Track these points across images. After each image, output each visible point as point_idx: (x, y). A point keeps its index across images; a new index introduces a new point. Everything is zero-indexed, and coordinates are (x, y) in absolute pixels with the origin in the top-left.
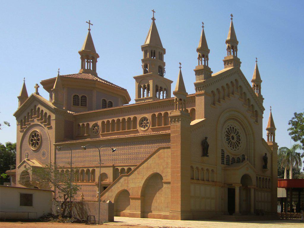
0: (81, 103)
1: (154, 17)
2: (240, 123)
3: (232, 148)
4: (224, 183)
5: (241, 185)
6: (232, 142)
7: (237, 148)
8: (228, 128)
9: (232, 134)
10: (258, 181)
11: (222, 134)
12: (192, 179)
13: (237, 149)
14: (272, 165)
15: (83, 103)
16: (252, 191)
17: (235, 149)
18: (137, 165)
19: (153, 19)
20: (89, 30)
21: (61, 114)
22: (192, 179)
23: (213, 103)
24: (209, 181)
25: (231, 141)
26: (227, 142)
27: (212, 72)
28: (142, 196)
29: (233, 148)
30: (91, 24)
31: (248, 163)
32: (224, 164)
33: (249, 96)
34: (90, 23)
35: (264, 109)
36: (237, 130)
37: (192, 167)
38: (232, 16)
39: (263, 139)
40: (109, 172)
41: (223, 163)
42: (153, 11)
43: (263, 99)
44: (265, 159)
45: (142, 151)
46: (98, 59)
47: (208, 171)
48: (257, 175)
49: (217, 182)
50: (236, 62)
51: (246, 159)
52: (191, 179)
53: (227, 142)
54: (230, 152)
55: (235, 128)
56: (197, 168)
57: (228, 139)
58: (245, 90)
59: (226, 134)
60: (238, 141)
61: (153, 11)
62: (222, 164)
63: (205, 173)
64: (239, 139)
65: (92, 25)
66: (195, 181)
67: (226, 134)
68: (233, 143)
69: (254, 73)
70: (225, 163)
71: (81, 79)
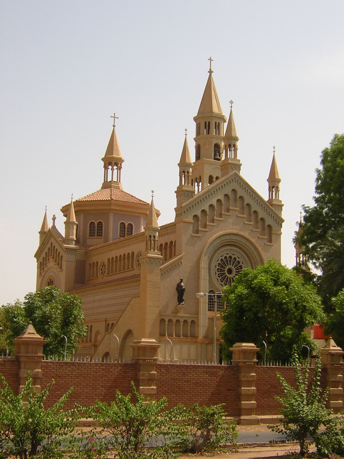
1: (210, 69)
8: (226, 257)
15: (99, 232)
19: (211, 72)
25: (228, 277)
30: (116, 118)
34: (114, 117)
42: (211, 60)
61: (211, 60)
65: (118, 118)
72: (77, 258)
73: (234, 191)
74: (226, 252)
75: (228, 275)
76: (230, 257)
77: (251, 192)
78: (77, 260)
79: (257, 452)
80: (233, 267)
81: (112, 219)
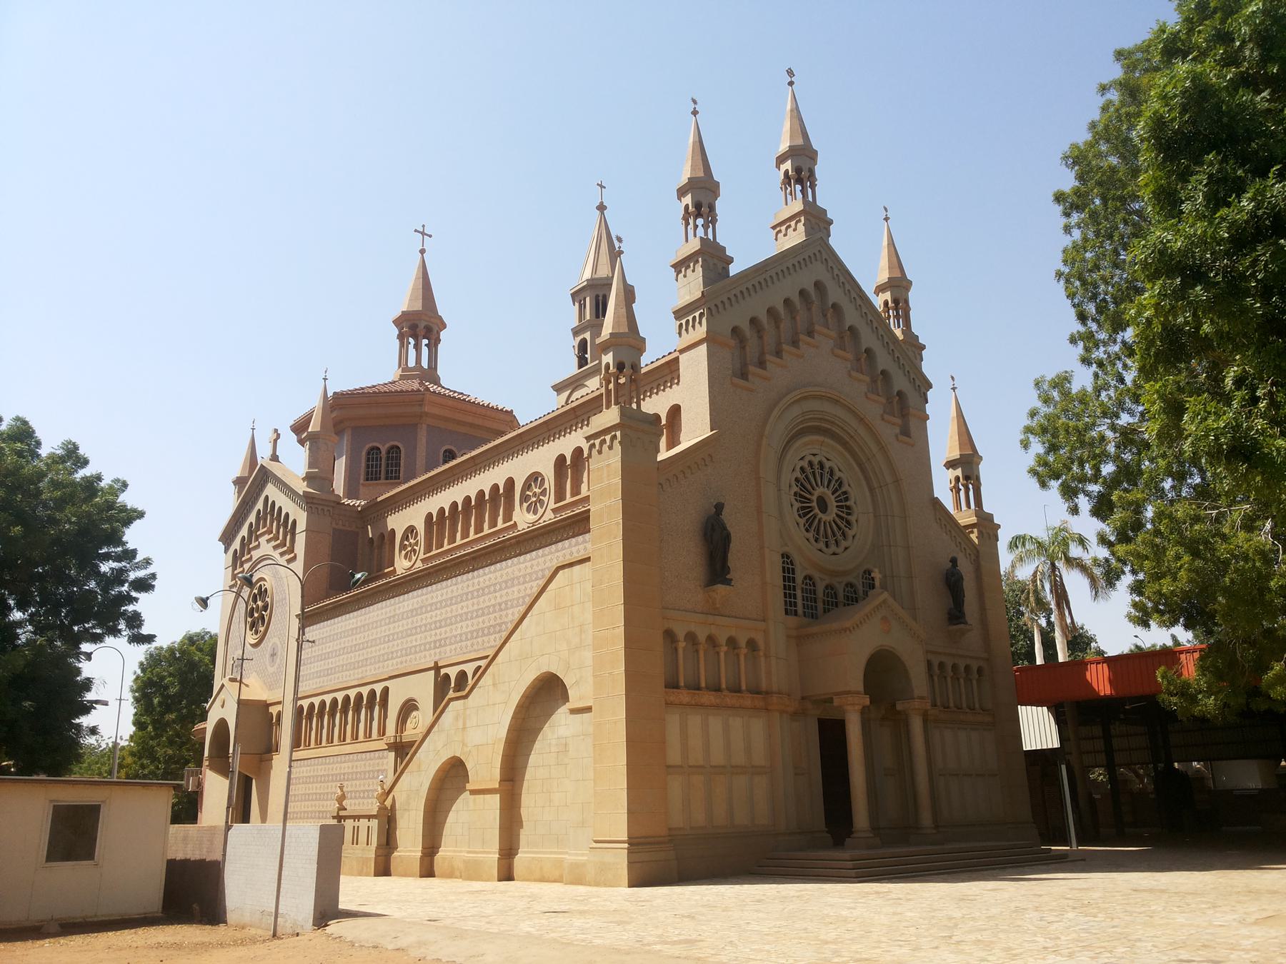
0: (387, 472)
1: (602, 203)
2: (844, 444)
3: (822, 545)
4: (803, 698)
5: (866, 700)
6: (820, 521)
7: (844, 544)
8: (802, 469)
9: (819, 491)
10: (936, 678)
11: (779, 490)
12: (672, 685)
13: (841, 549)
14: (983, 609)
16: (917, 725)
17: (833, 548)
18: (488, 656)
20: (422, 251)
21: (322, 509)
22: (672, 685)
23: (742, 374)
24: (739, 691)
26: (802, 521)
27: (730, 260)
28: (505, 781)
29: (827, 546)
30: (427, 235)
31: (884, 601)
32: (796, 614)
33: (868, 339)
34: (423, 234)
35: (930, 386)
36: (838, 474)
37: (670, 635)
38: (790, 73)
39: (937, 503)
40: (423, 689)
41: (790, 609)
43: (923, 347)
44: (952, 583)
45: (516, 595)
46: (443, 334)
47: (734, 648)
48: (927, 652)
49: (772, 693)
50: (817, 221)
51: (877, 583)
52: (666, 687)
53: (802, 521)
54: (808, 554)
55: (827, 465)
56: (691, 637)
57: (805, 511)
58: (851, 317)
59: (795, 489)
60: (842, 518)
62: (787, 613)
63: (722, 655)
64: (848, 508)
65: (430, 236)
66: (685, 696)
67: (795, 489)
68: (829, 523)
69: (884, 262)
70: (800, 609)
71: (386, 392)
72: (337, 524)
73: (818, 285)
74: (812, 448)
75: (824, 517)
76: (821, 465)
77: (857, 298)
78: (334, 529)
79: (104, 912)
80: (829, 493)
81: (424, 440)
